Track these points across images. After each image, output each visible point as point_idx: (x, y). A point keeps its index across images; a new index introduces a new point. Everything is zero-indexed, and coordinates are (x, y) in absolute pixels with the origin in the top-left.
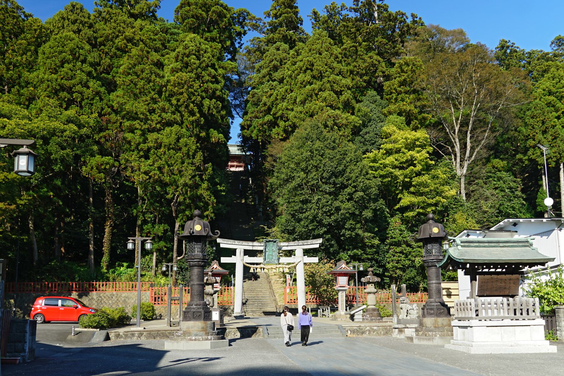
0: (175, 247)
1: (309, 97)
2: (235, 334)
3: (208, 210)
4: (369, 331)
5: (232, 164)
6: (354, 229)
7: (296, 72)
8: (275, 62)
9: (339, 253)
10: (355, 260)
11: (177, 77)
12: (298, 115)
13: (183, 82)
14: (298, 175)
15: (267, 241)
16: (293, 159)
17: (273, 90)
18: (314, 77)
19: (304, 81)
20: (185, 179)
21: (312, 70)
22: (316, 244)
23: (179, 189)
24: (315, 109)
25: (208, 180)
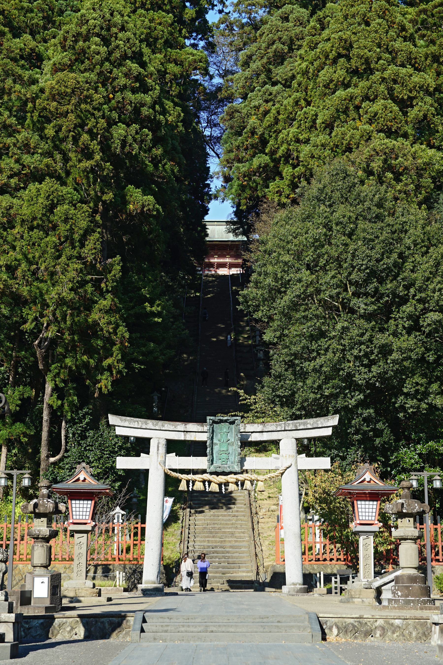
0: (44, 435)
1: (343, 112)
2: (72, 629)
3: (112, 355)
4: (383, 628)
5: (221, 260)
6: (426, 394)
7: (316, 64)
8: (278, 46)
9: (397, 449)
10: (433, 465)
11: (58, 82)
12: (317, 152)
13: (69, 90)
14: (298, 276)
15: (214, 422)
16: (288, 243)
17: (270, 104)
18: (355, 72)
19: (332, 81)
20: (63, 290)
21: (349, 59)
22: (324, 426)
23: (48, 312)
24: (352, 137)
25: (114, 291)
